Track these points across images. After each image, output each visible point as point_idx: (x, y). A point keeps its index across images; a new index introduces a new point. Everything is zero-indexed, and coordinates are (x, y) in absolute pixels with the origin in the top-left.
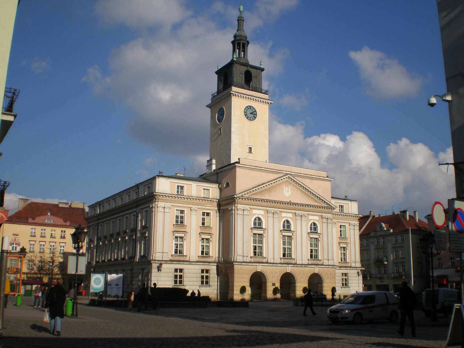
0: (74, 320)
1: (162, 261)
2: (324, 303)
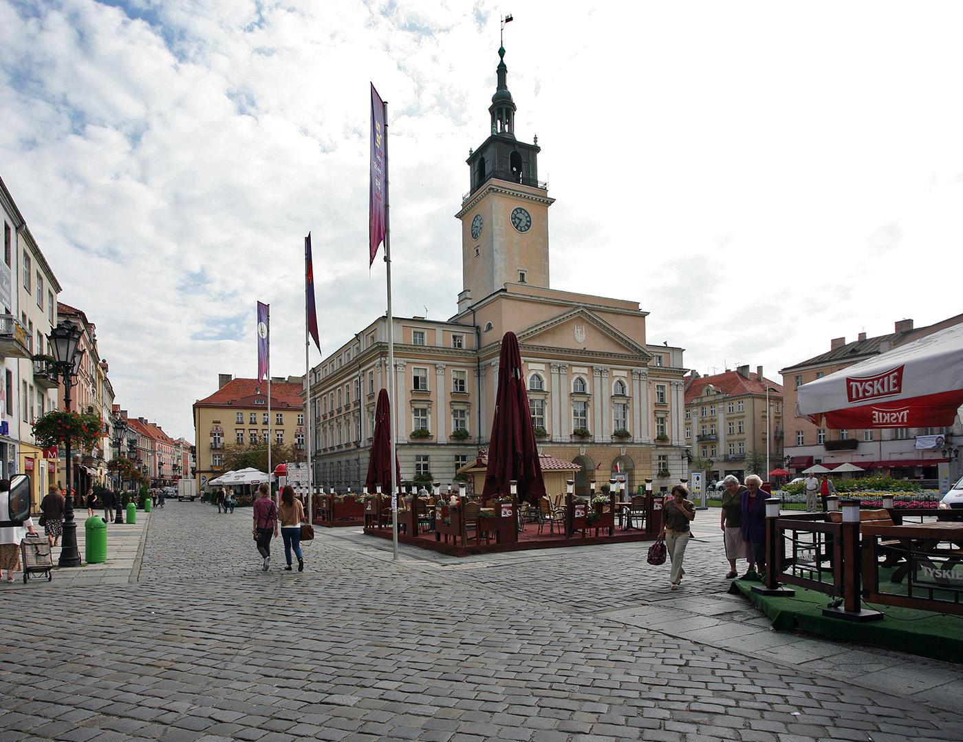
0: (91, 567)
2: (427, 441)
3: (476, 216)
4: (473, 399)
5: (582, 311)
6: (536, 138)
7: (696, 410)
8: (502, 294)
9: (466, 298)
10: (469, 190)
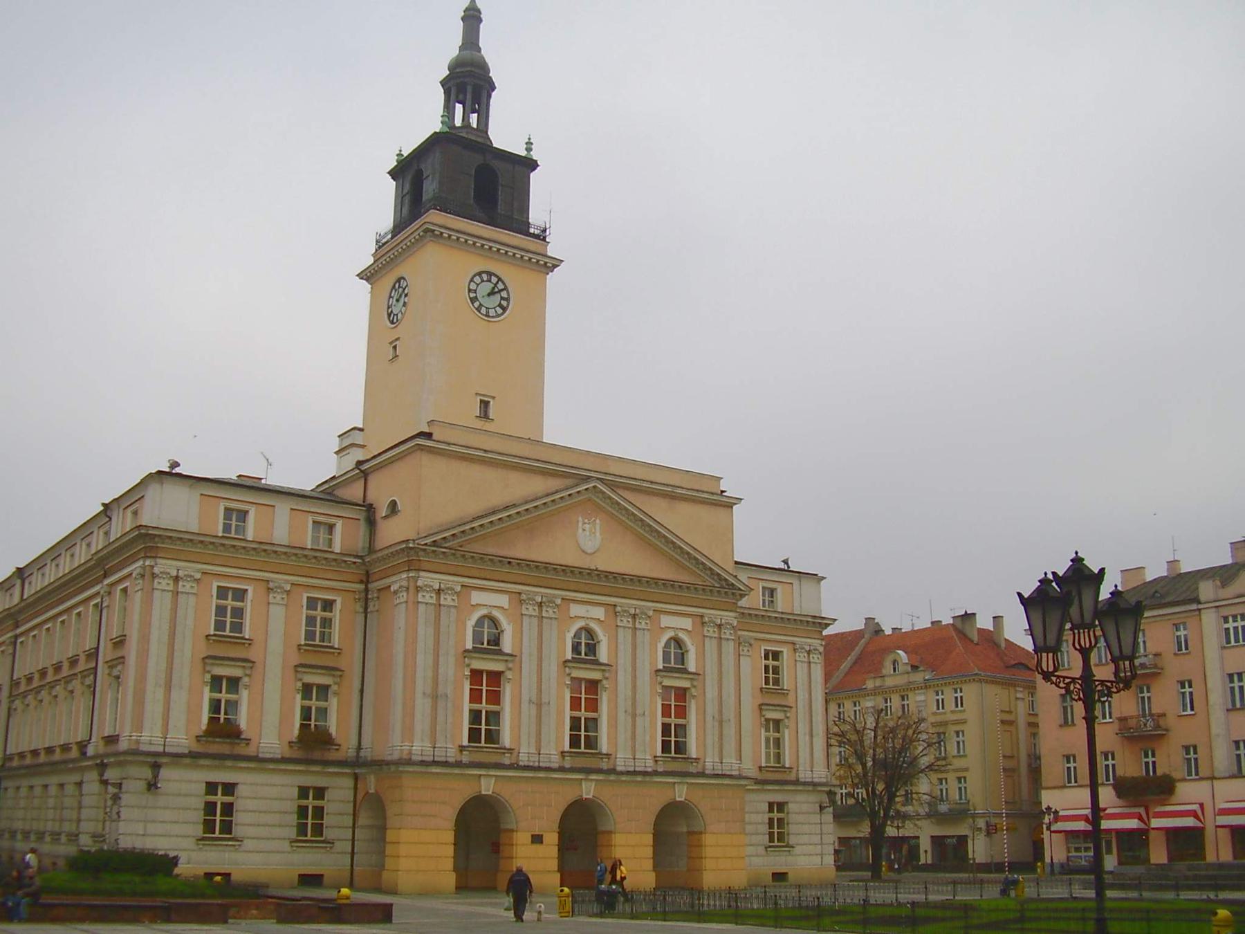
1: (164, 754)
3: (399, 280)
4: (350, 663)
6: (529, 143)
7: (922, 698)
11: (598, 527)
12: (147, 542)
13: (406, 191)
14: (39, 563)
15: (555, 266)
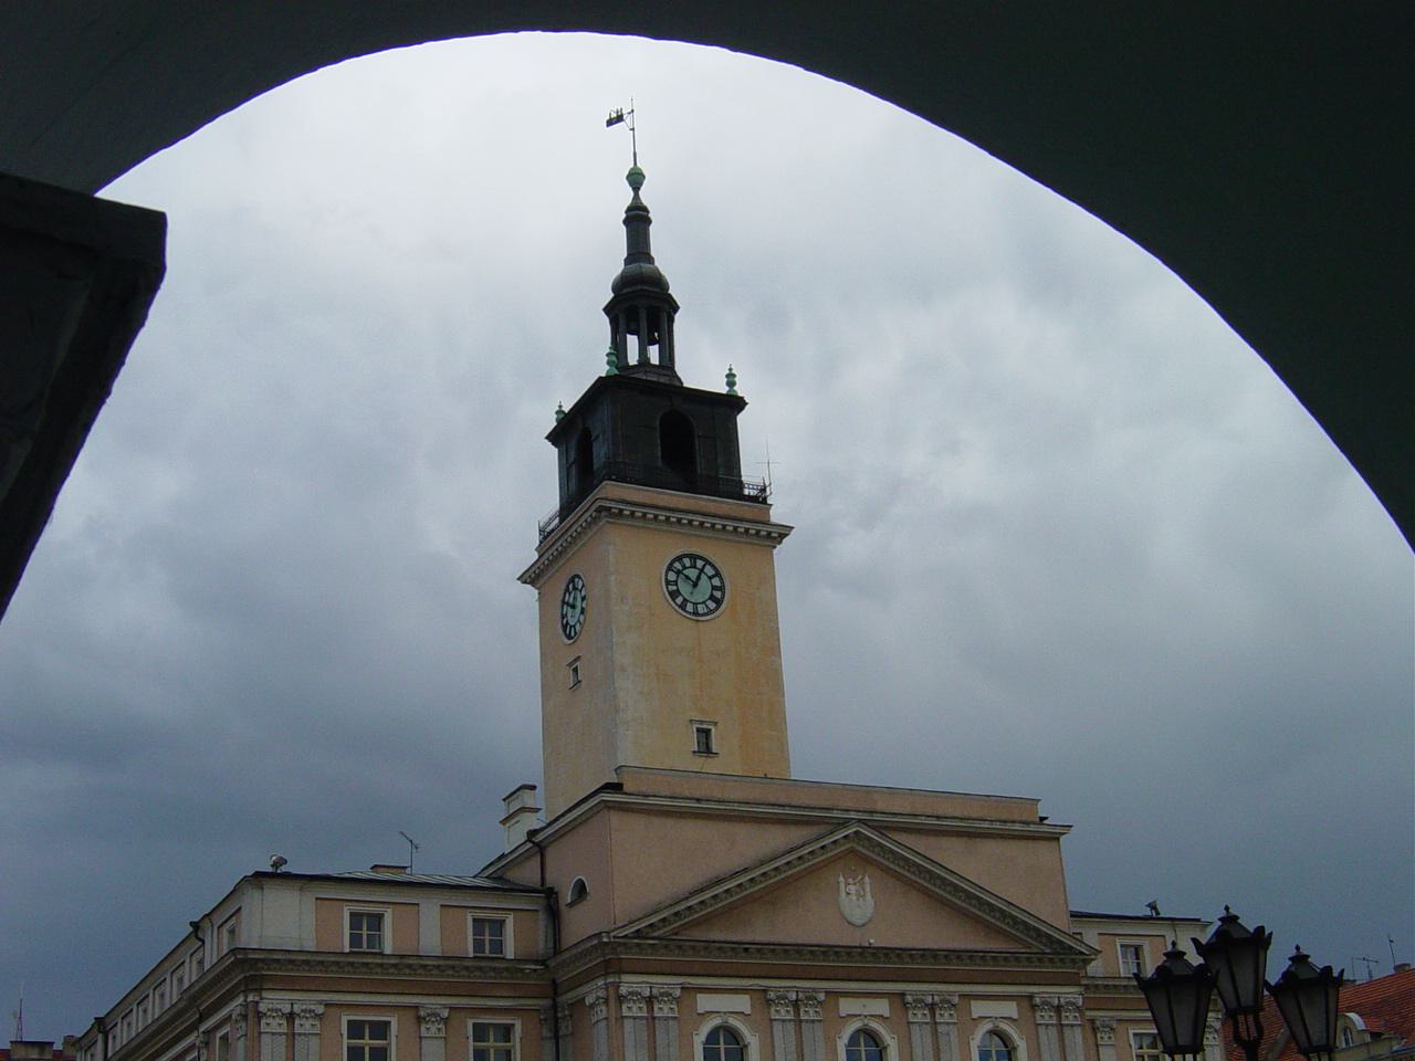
3: (572, 580)
5: (856, 833)
8: (607, 797)
9: (523, 810)
10: (558, 507)
11: (868, 888)
12: (252, 971)
13: (571, 460)
14: (123, 1008)
15: (782, 536)
